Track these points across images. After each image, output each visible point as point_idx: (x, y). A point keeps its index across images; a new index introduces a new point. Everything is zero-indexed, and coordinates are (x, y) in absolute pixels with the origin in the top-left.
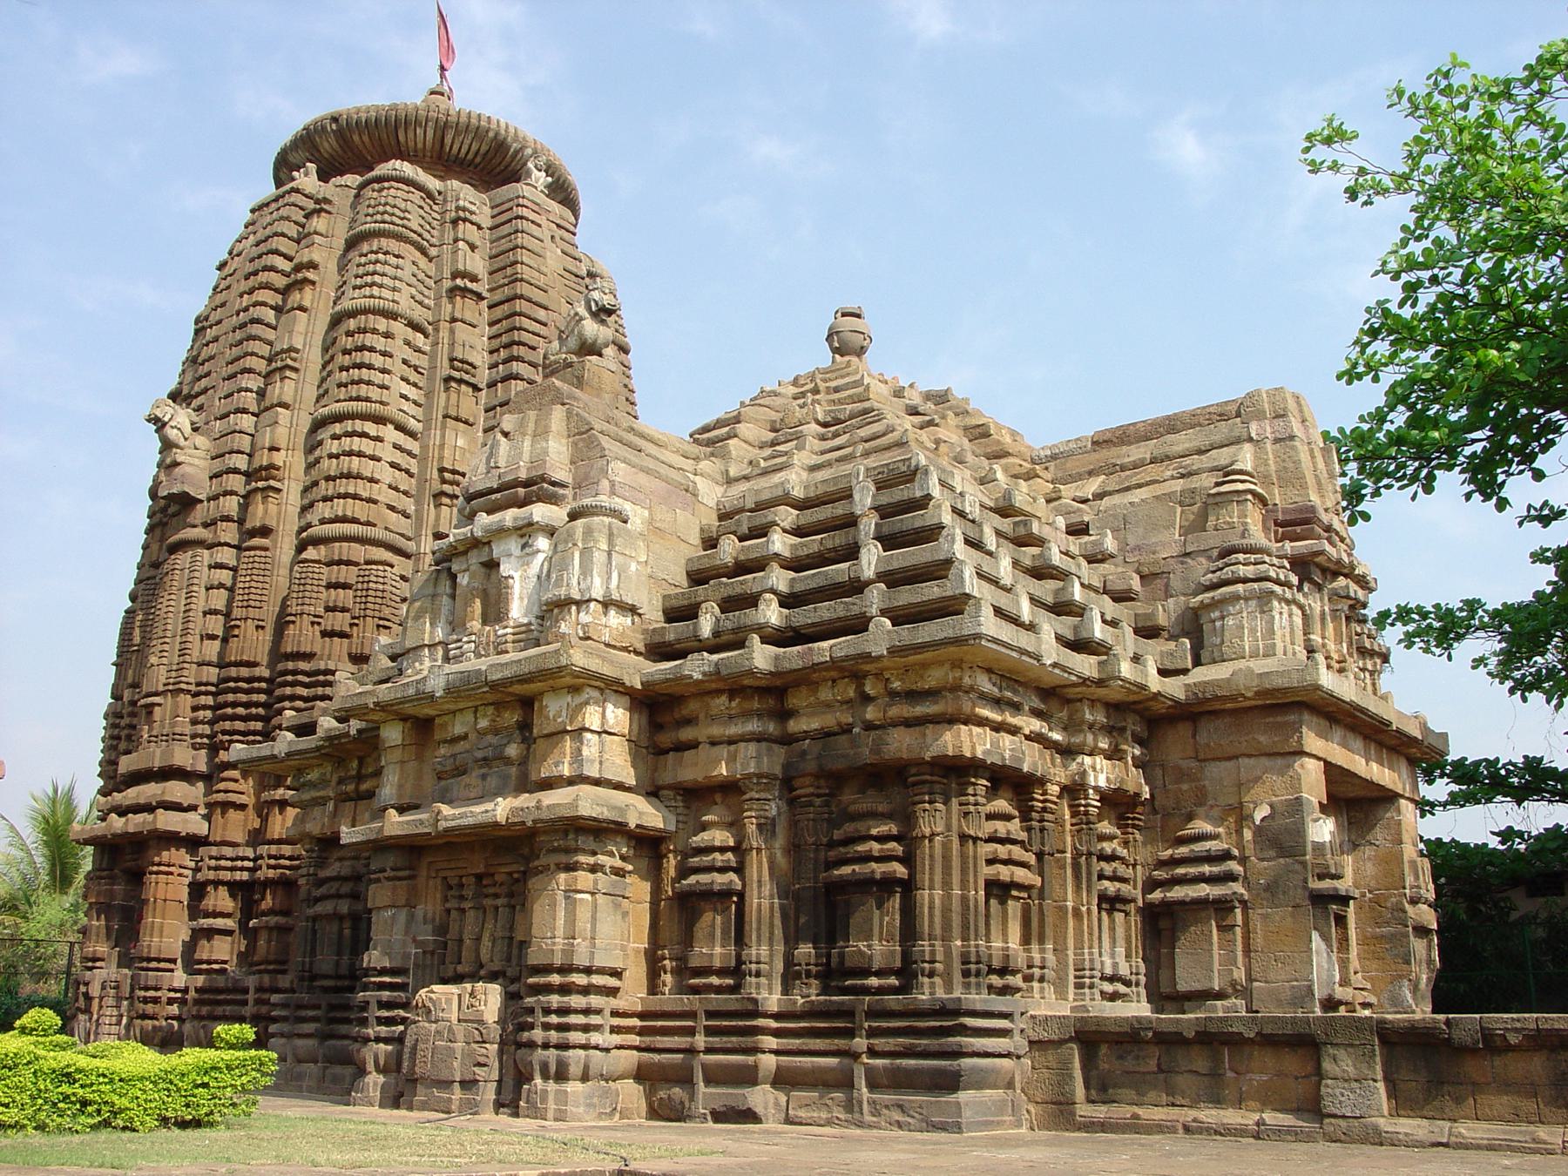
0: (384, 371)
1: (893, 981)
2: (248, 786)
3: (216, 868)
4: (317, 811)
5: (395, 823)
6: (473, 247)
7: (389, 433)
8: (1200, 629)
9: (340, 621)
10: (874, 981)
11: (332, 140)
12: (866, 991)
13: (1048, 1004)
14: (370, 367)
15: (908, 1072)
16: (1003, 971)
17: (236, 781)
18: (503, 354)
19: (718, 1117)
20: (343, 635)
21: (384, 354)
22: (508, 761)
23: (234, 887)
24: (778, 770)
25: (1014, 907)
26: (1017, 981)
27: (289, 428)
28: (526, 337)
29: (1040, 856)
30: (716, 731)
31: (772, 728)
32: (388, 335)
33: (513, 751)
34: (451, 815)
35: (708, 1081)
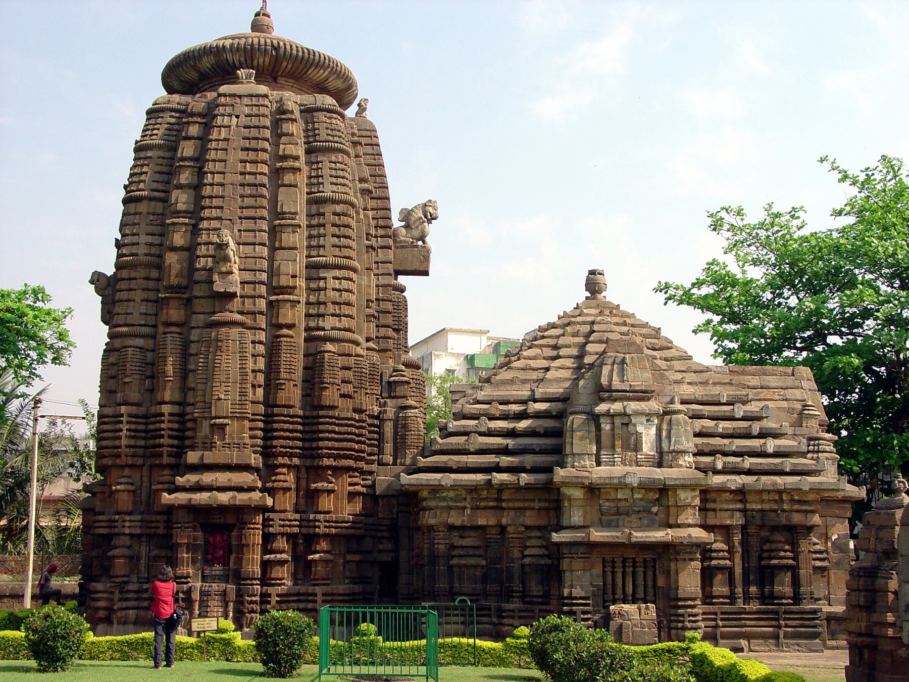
1: (790, 601)
2: (291, 478)
3: (283, 526)
9: (348, 389)
10: (785, 601)
11: (267, 60)
12: (782, 604)
15: (801, 632)
17: (284, 474)
20: (349, 397)
23: (290, 537)
30: (725, 506)
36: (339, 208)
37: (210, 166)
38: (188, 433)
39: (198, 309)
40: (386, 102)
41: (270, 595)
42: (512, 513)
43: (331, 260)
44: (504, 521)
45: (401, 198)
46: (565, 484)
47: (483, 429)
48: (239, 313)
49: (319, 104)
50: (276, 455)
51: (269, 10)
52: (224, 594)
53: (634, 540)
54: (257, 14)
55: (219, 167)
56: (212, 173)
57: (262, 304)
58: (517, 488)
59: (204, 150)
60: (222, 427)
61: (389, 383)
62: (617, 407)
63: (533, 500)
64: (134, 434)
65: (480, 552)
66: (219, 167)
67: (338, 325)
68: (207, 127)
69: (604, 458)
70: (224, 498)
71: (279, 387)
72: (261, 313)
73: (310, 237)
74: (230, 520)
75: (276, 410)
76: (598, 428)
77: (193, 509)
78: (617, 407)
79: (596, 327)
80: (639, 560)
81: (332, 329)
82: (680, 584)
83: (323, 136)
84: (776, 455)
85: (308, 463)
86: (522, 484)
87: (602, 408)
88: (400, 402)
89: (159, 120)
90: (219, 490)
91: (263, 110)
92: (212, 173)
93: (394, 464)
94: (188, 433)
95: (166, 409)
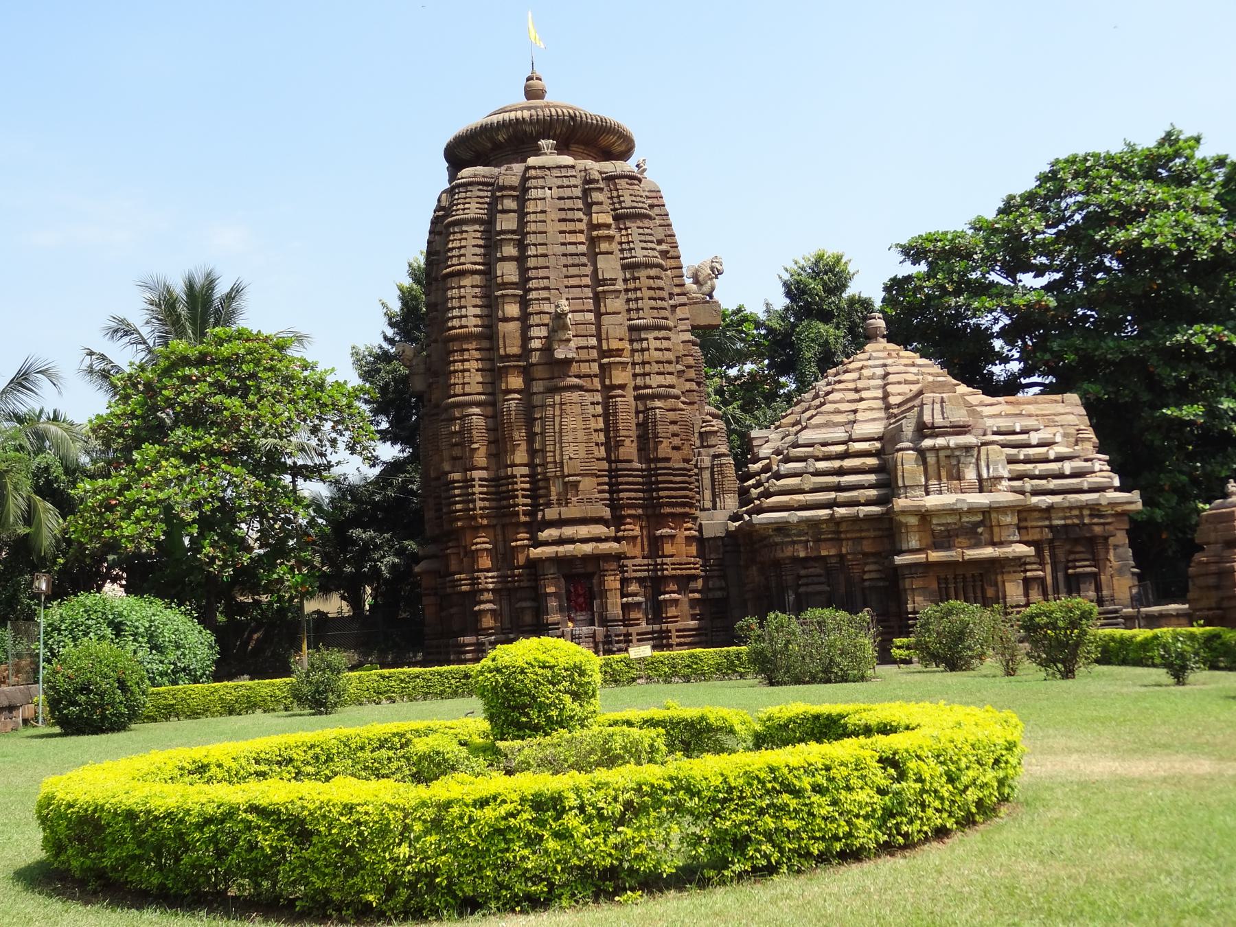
9: (676, 441)
30: (1035, 524)
36: (653, 272)
37: (531, 239)
38: (541, 492)
39: (537, 375)
40: (656, 160)
41: (631, 635)
42: (850, 543)
43: (651, 321)
44: (844, 551)
45: (691, 257)
46: (904, 512)
47: (811, 470)
48: (576, 377)
49: (619, 171)
50: (623, 507)
51: (538, 73)
52: (594, 636)
53: (966, 558)
54: (529, 79)
55: (540, 238)
56: (535, 245)
57: (595, 368)
58: (855, 520)
59: (522, 223)
60: (575, 485)
61: (700, 433)
62: (940, 441)
63: (868, 530)
64: (487, 496)
65: (822, 579)
66: (540, 238)
67: (664, 383)
68: (522, 200)
69: (932, 488)
70: (588, 548)
71: (619, 444)
72: (596, 376)
73: (628, 301)
74: (590, 569)
75: (620, 465)
76: (925, 463)
77: (557, 560)
78: (940, 441)
79: (890, 369)
80: (969, 575)
81: (659, 386)
82: (1008, 593)
83: (628, 203)
84: (1073, 475)
85: (650, 511)
86: (861, 515)
87: (928, 443)
88: (712, 451)
89: (469, 194)
90: (587, 541)
91: (573, 181)
92: (535, 245)
93: (714, 508)
94: (541, 492)
95: (519, 471)
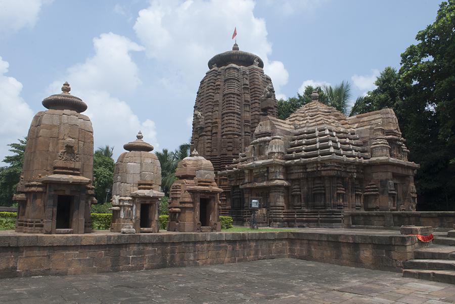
0: (234, 104)
4: (233, 182)
5: (248, 186)
6: (247, 79)
7: (236, 115)
8: (372, 152)
9: (231, 148)
13: (347, 211)
14: (231, 104)
16: (340, 206)
18: (253, 99)
19: (299, 227)
21: (234, 101)
22: (265, 176)
24: (306, 177)
25: (341, 197)
26: (342, 207)
27: (217, 114)
28: (258, 95)
29: (345, 189)
30: (296, 171)
31: (304, 171)
32: (234, 98)
33: (266, 175)
34: (257, 184)
35: (297, 222)
